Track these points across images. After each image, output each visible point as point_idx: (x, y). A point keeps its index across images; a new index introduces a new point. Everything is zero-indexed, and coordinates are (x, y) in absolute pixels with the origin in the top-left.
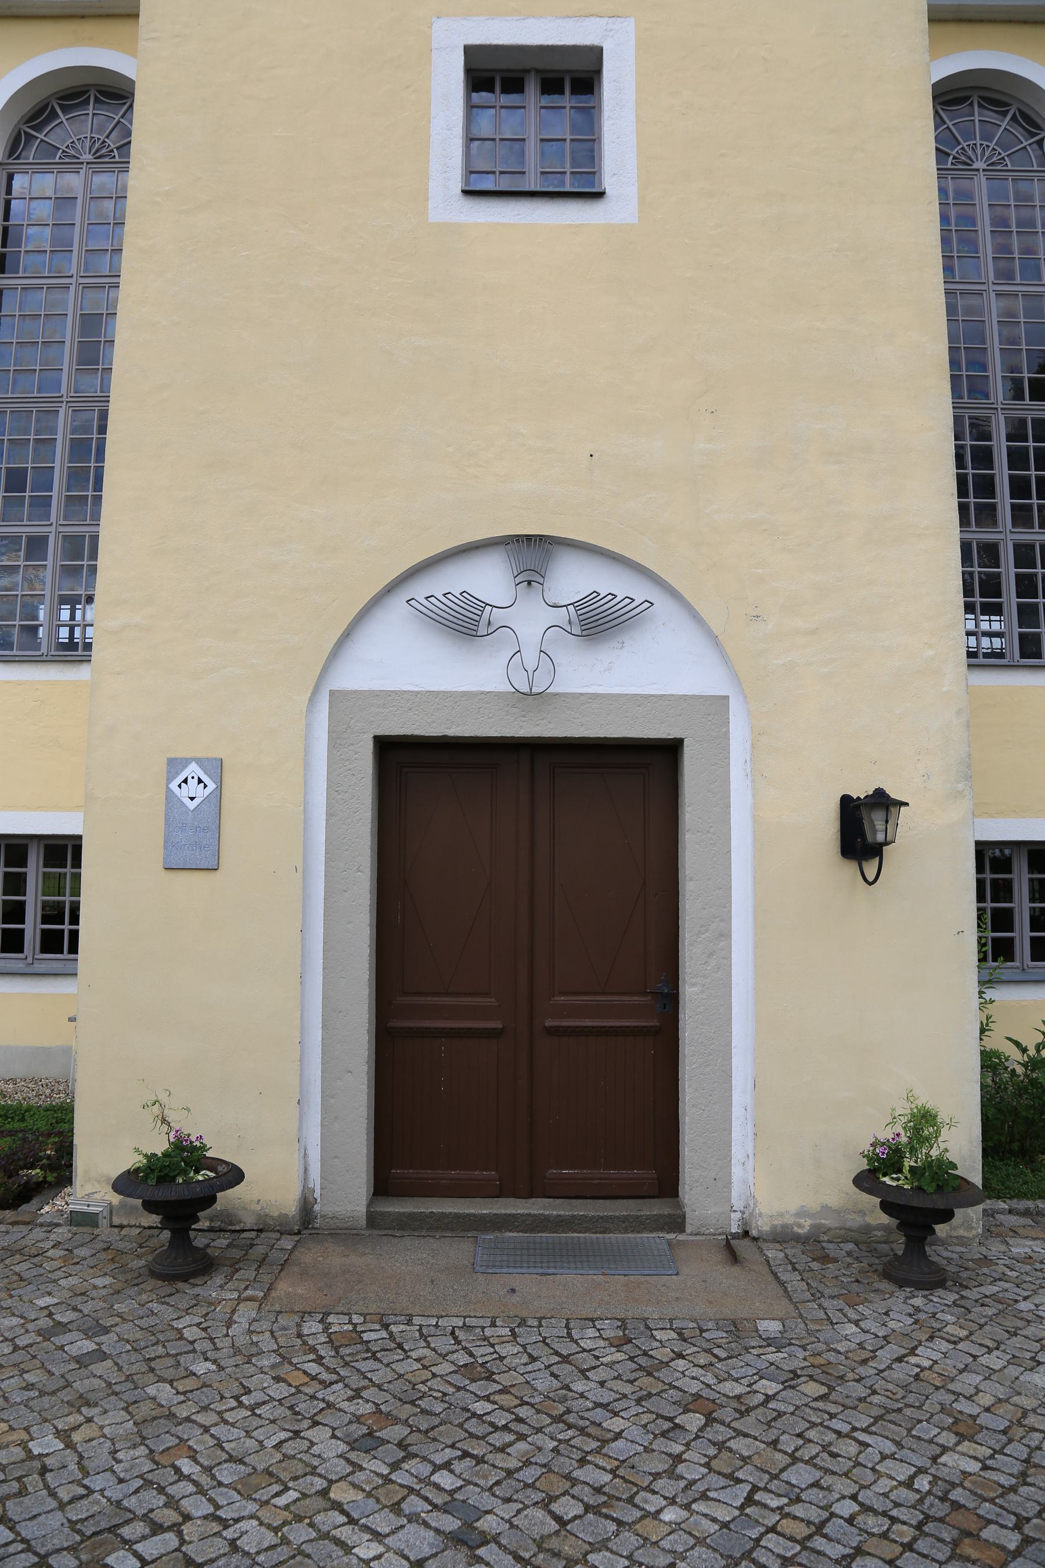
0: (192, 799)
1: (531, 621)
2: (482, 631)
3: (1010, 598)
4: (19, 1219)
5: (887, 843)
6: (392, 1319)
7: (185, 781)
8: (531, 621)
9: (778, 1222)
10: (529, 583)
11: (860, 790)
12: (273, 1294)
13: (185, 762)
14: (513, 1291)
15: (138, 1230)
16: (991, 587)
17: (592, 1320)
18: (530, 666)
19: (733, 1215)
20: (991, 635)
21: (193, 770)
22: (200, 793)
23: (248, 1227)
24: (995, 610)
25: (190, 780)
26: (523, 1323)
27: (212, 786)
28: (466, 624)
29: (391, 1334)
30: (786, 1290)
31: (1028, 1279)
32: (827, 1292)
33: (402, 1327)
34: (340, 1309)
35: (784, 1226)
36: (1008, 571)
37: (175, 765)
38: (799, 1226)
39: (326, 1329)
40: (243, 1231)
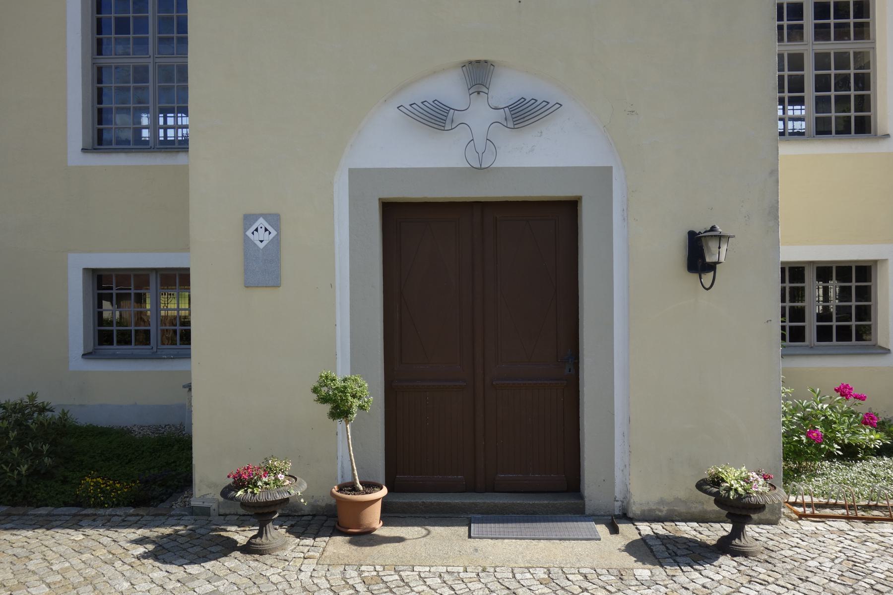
0: (261, 241)
1: (480, 116)
2: (448, 127)
3: (810, 92)
4: (160, 512)
5: (718, 263)
6: (401, 568)
7: (256, 230)
8: (480, 116)
9: (646, 508)
10: (479, 93)
11: (700, 227)
12: (325, 554)
13: (256, 217)
14: (476, 550)
15: (236, 517)
16: (797, 85)
17: (528, 568)
18: (480, 150)
19: (616, 503)
20: (794, 119)
21: (261, 222)
22: (267, 238)
23: (306, 513)
24: (800, 101)
25: (259, 229)
26: (484, 570)
27: (274, 233)
28: (437, 117)
29: (400, 576)
30: (652, 551)
31: (814, 546)
32: (679, 552)
33: (409, 573)
34: (368, 562)
35: (650, 510)
36: (809, 74)
37: (249, 219)
38: (660, 511)
39: (360, 575)
40: (303, 516)
